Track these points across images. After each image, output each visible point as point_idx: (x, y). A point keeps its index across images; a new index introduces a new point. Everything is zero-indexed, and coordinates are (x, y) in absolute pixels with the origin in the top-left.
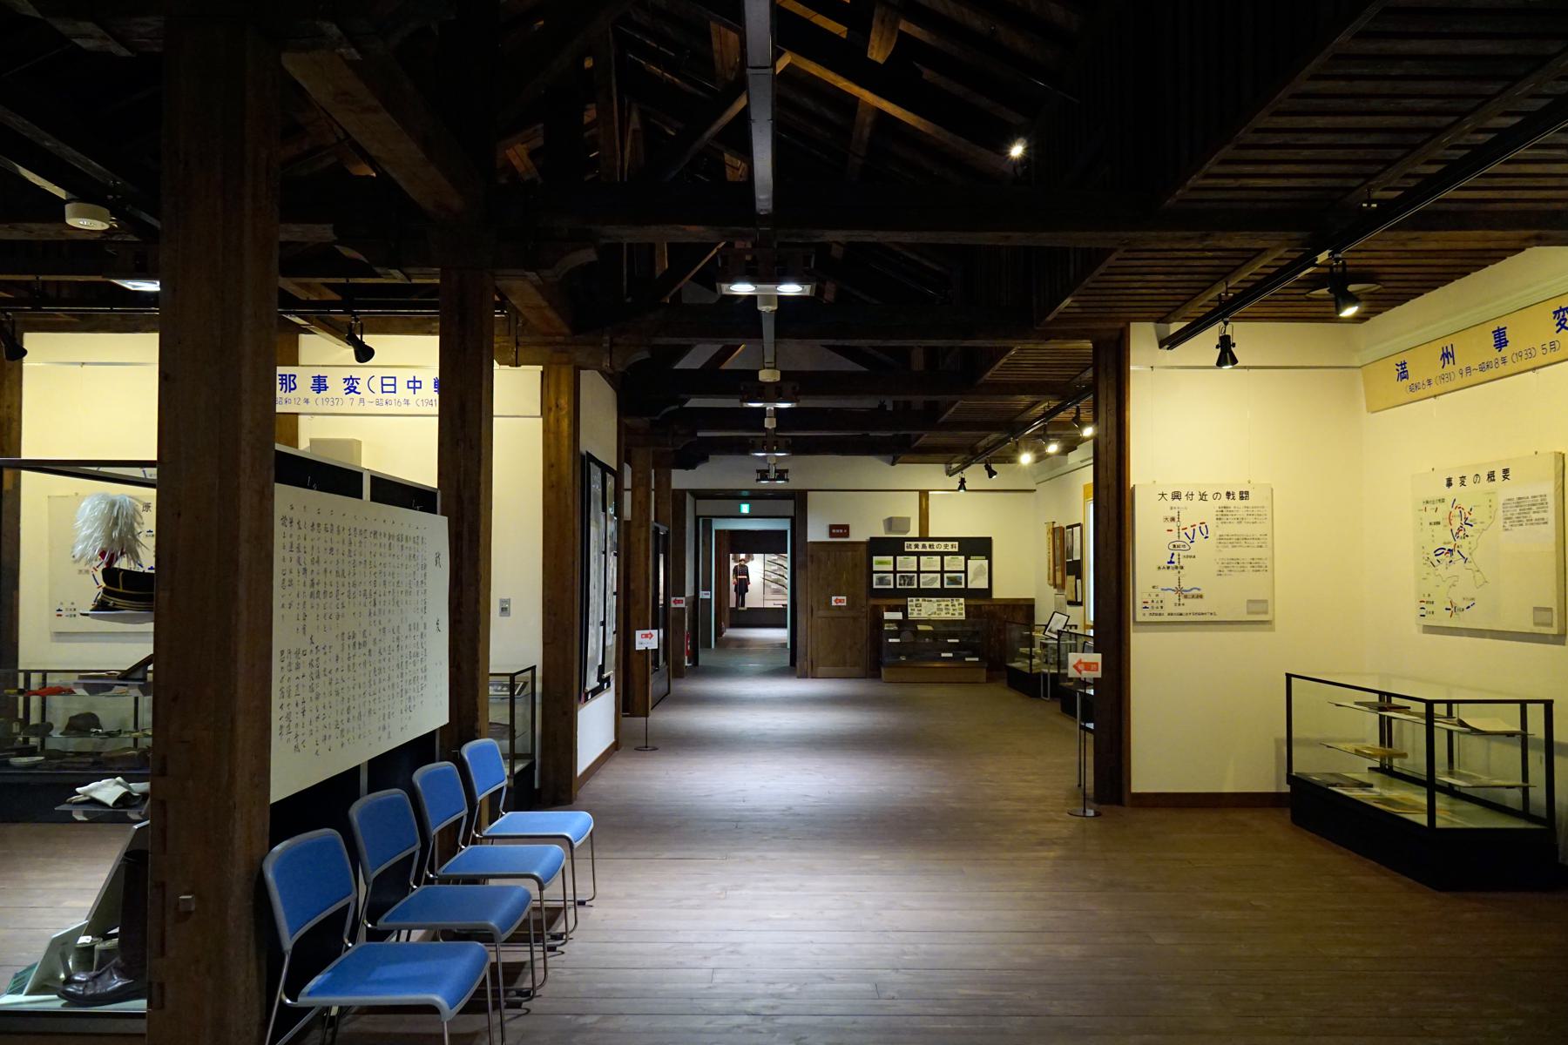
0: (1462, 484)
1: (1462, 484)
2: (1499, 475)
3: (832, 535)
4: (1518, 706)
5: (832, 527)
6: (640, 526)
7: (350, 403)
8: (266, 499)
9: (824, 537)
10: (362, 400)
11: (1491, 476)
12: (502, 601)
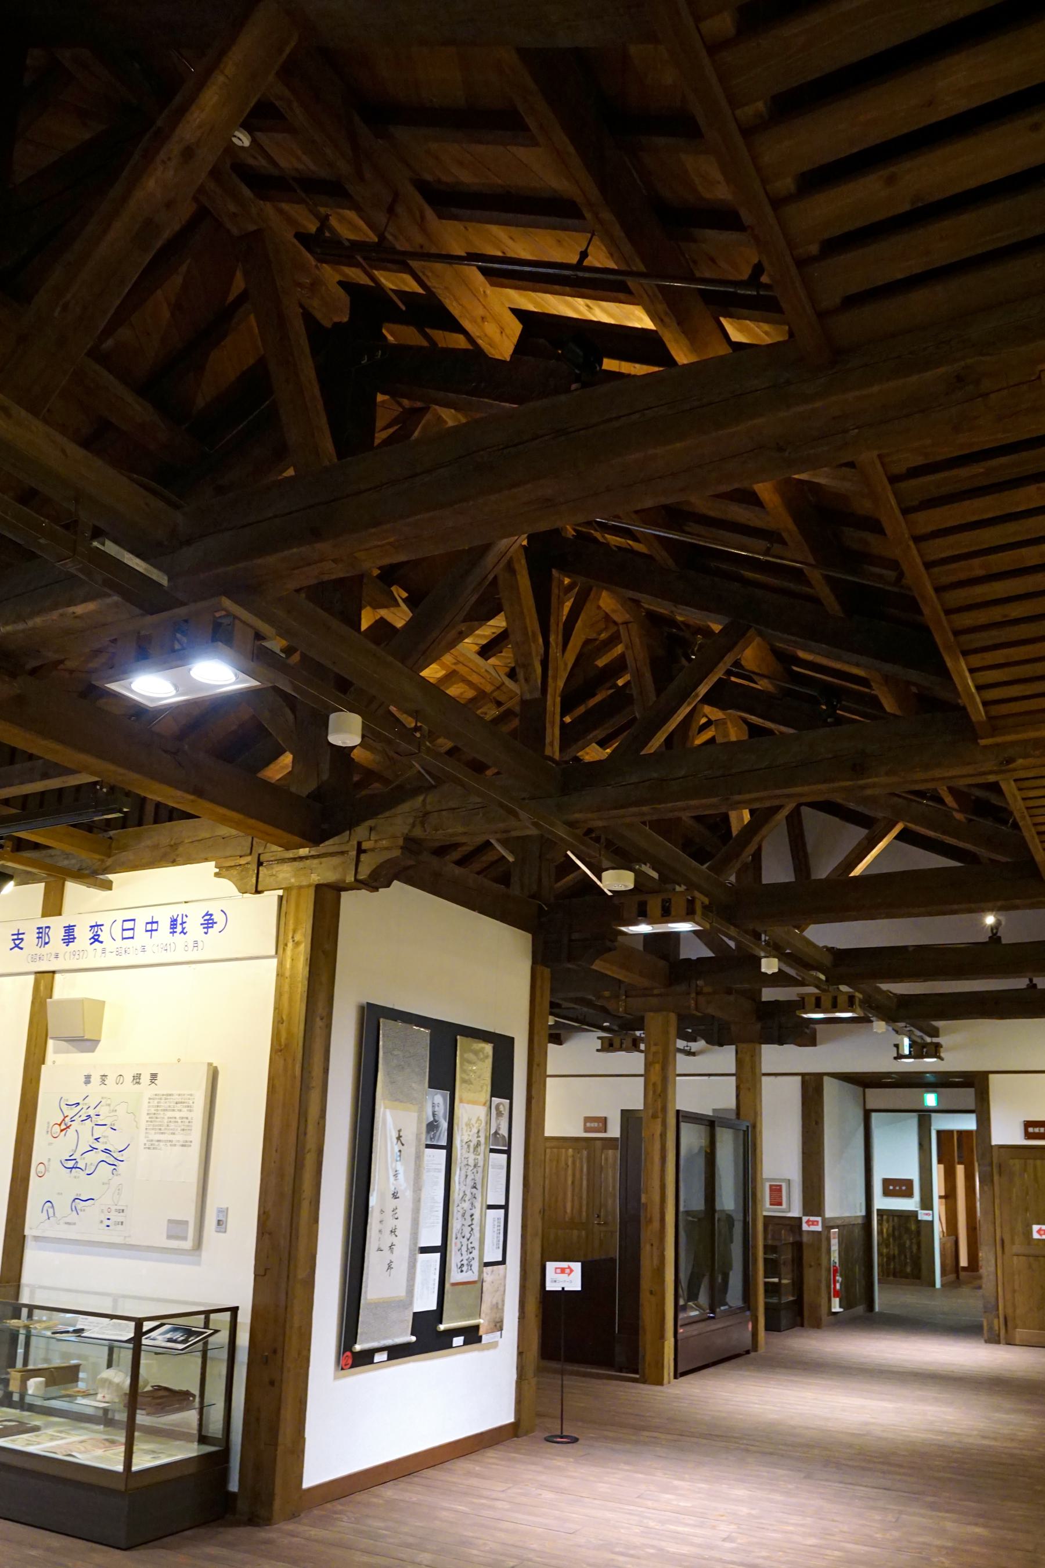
0: (103, 1082)
1: (103, 1082)
2: (145, 1079)
3: (1028, 1136)
4: (503, 1203)
5: (1028, 1124)
6: (654, 1116)
7: (94, 956)
8: (675, 1056)
9: (1017, 1138)
10: (104, 950)
11: (137, 1079)
12: (220, 1211)
